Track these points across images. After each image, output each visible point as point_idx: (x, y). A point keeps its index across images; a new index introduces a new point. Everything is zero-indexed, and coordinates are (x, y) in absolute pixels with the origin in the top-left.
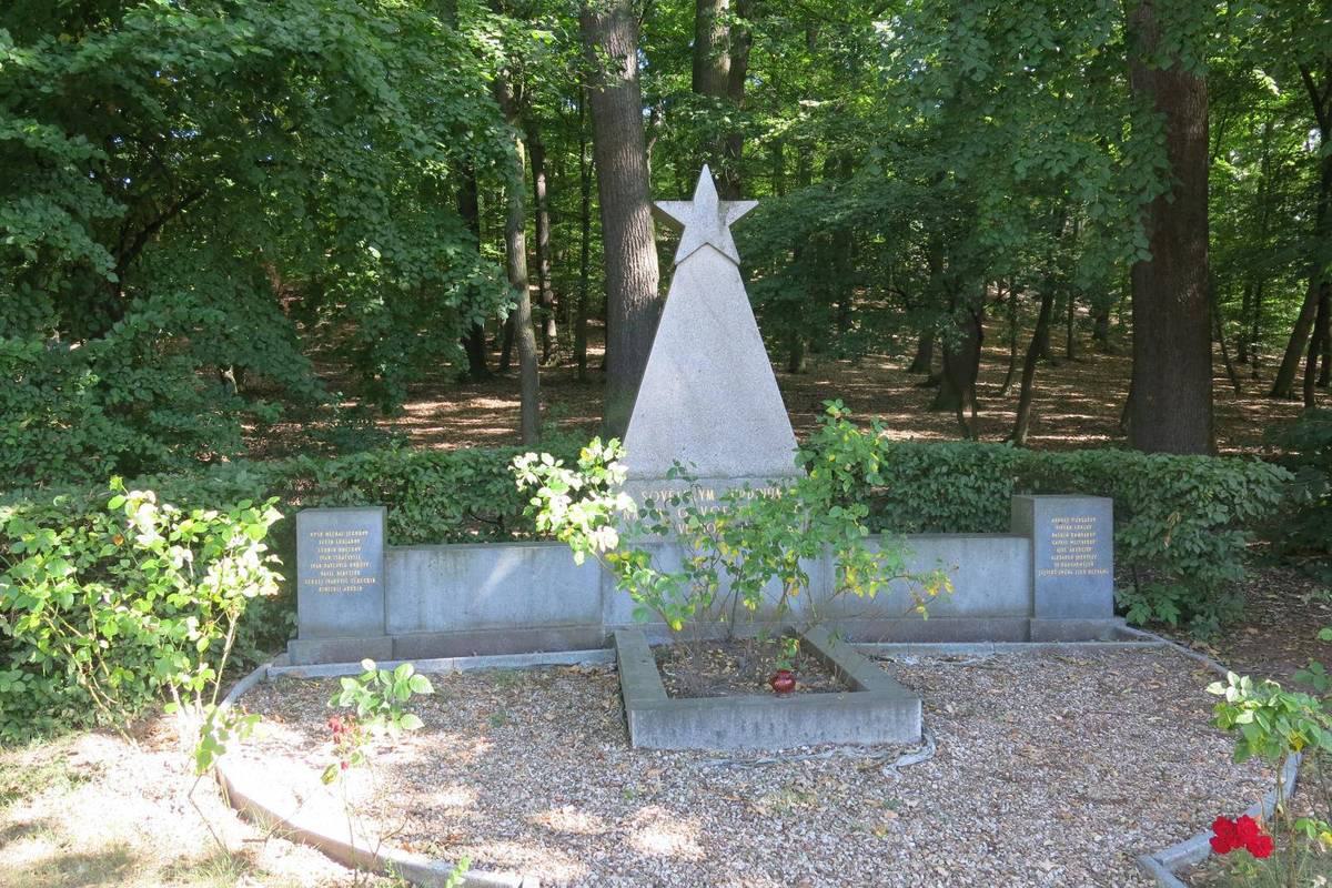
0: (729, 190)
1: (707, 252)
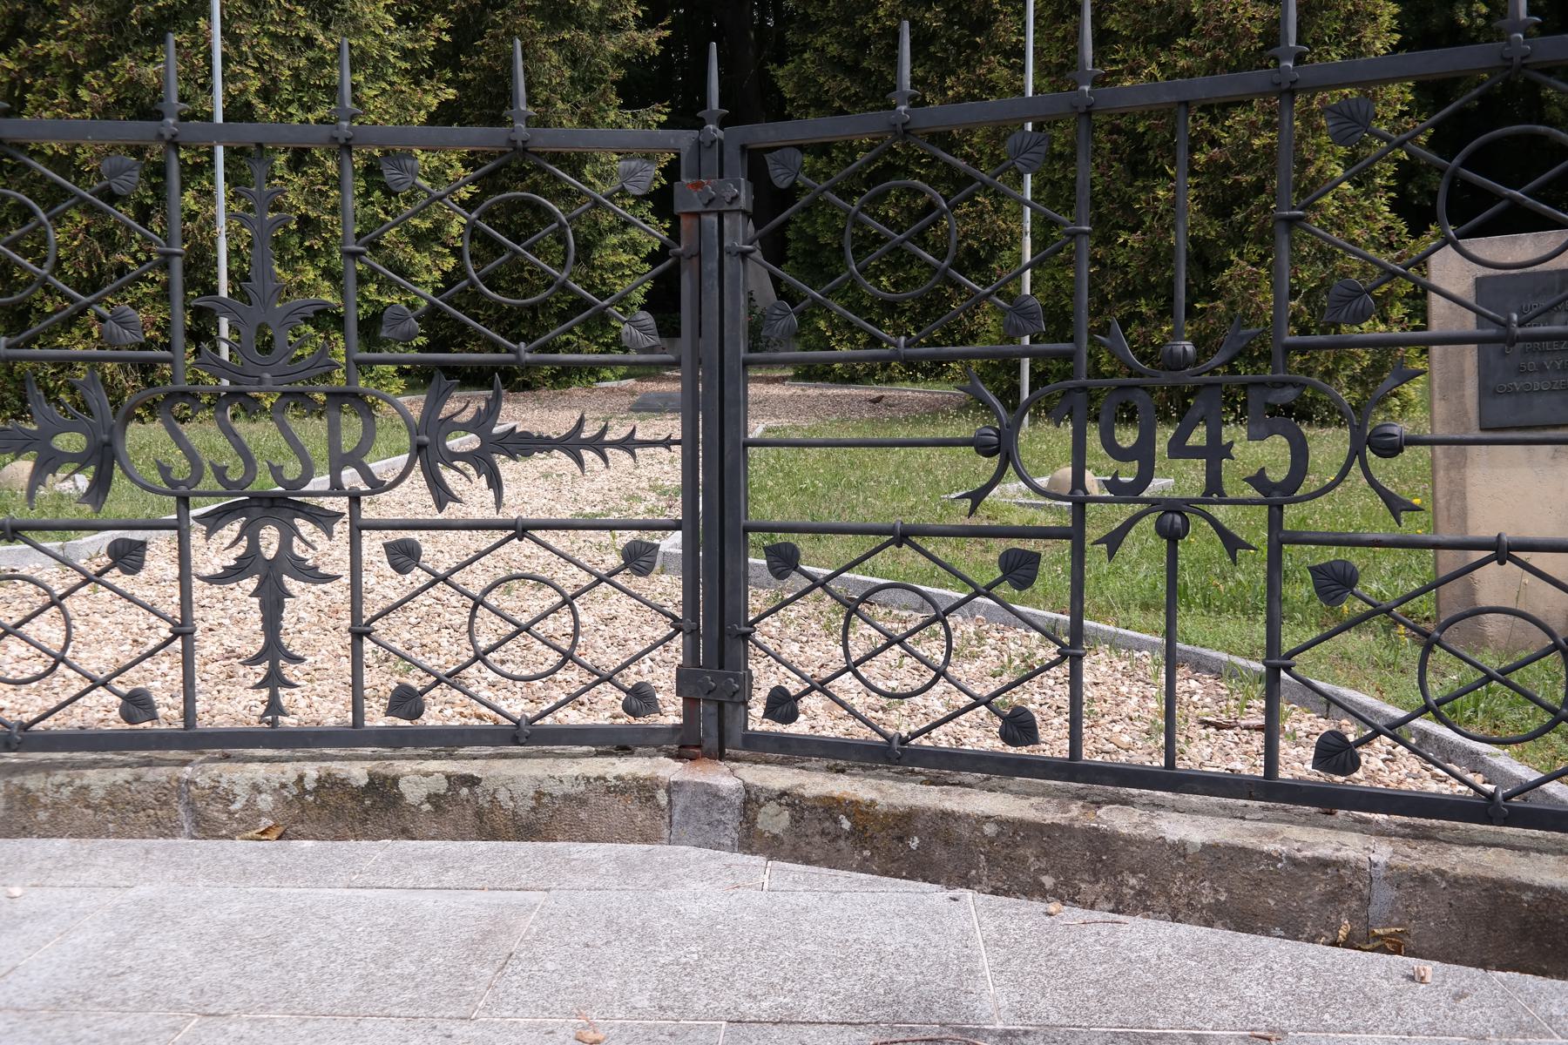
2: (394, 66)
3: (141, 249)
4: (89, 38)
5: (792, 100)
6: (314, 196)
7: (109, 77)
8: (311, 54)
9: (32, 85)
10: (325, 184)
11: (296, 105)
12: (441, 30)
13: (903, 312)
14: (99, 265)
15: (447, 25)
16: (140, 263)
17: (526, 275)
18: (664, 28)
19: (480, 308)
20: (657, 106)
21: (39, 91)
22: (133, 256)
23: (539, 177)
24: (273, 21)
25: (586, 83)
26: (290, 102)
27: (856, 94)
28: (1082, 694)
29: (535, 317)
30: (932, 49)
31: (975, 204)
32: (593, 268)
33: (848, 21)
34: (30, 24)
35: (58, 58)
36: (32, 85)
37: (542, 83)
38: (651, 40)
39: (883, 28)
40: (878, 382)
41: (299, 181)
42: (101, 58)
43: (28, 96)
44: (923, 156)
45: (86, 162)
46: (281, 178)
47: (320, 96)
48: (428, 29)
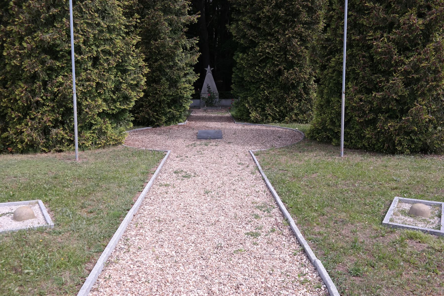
0: (211, 67)
2: (123, 31)
3: (44, 95)
4: (26, 25)
5: (236, 36)
6: (101, 76)
7: (33, 38)
8: (98, 28)
9: (6, 41)
10: (104, 72)
11: (94, 45)
12: (137, 19)
13: (271, 102)
14: (30, 101)
15: (139, 17)
16: (44, 100)
17: (158, 92)
18: (198, 14)
19: (144, 102)
20: (195, 38)
21: (9, 43)
22: (42, 97)
23: (162, 62)
24: (87, 18)
25: (174, 31)
26: (92, 45)
29: (160, 104)
30: (280, 22)
31: (294, 69)
32: (178, 89)
33: (253, 12)
34: (5, 19)
35: (15, 32)
36: (6, 41)
37: (163, 32)
38: (195, 18)
39: (265, 15)
40: (265, 123)
41: (96, 71)
42: (30, 32)
43: (5, 45)
44: (278, 55)
45: (25, 68)
46: (90, 70)
47: (102, 42)
48: (133, 18)
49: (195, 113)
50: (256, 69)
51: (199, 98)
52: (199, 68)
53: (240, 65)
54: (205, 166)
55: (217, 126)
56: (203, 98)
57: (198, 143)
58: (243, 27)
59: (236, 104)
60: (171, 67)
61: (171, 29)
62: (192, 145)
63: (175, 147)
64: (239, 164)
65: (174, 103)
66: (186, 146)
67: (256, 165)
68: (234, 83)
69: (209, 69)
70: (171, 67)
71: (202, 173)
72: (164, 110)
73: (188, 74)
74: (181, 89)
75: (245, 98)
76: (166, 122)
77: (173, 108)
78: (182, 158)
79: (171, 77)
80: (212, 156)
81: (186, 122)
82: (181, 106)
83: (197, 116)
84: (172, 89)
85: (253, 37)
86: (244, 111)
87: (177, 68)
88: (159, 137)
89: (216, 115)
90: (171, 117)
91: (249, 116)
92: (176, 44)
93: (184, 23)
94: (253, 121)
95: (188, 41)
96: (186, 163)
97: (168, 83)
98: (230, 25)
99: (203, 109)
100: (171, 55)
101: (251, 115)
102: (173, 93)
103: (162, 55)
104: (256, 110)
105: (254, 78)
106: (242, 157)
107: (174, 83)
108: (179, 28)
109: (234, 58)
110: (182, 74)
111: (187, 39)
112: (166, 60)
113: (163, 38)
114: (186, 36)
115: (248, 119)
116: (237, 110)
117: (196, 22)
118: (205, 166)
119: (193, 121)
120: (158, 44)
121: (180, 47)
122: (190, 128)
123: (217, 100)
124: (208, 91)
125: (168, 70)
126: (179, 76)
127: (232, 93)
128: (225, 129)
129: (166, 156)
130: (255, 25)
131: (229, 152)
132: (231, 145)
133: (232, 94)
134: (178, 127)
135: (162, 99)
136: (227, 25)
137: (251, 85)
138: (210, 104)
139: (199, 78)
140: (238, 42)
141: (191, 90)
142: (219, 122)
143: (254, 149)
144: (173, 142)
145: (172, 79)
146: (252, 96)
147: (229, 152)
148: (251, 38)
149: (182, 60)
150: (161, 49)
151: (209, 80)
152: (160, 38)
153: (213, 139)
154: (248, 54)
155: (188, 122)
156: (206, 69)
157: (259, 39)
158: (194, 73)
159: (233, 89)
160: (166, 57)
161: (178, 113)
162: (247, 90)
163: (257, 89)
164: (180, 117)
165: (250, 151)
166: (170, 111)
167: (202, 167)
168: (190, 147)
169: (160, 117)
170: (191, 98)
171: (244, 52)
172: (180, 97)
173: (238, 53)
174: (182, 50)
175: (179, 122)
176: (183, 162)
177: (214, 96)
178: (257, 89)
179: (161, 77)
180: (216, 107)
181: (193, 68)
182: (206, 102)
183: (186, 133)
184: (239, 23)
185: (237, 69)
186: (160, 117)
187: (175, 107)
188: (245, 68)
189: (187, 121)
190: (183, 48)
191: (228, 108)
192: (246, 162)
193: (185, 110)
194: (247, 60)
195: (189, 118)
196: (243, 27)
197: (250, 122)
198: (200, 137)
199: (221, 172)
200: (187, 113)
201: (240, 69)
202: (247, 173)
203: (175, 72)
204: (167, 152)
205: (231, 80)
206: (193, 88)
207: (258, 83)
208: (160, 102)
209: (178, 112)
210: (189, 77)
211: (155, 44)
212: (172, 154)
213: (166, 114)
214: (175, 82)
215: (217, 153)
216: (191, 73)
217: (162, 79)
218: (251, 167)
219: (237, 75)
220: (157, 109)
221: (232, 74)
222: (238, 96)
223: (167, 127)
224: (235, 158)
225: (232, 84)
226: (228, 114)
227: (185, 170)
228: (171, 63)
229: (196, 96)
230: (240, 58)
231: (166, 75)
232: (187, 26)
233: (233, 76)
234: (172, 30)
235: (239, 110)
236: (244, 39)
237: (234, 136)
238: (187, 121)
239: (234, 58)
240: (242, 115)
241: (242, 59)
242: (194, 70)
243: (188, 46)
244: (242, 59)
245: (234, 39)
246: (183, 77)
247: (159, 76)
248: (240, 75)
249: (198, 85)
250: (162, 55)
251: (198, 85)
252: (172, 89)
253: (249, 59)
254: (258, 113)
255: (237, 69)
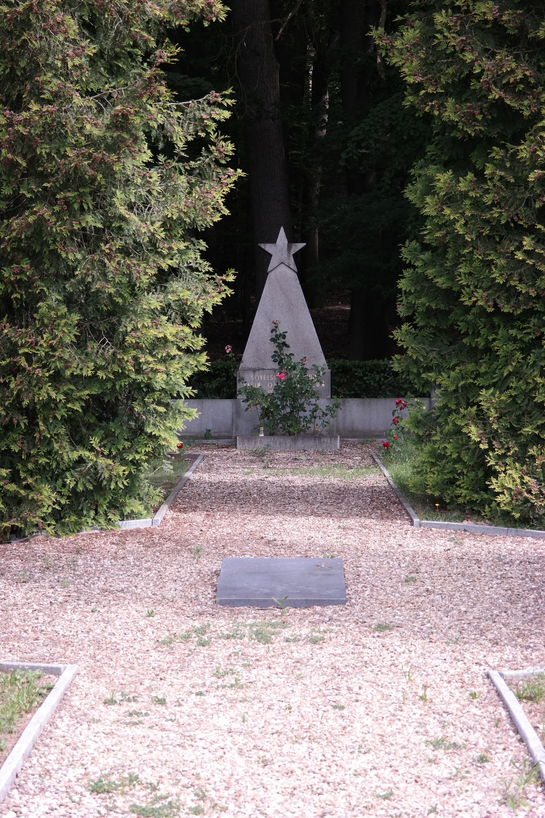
0: (291, 240)
1: (283, 268)
5: (419, 86)
17: (23, 362)
20: (213, 96)
23: (45, 211)
25: (110, 63)
27: (525, 80)
28: (243, 606)
29: (33, 424)
32: (123, 347)
37: (52, 67)
49: (209, 469)
50: (520, 247)
51: (232, 395)
52: (232, 247)
53: (440, 227)
54: (255, 755)
55: (319, 538)
56: (252, 394)
57: (222, 624)
58: (455, 41)
59: (418, 423)
60: (89, 240)
61: (92, 50)
62: (186, 638)
63: (98, 644)
64: (437, 744)
65: (100, 419)
66: (160, 644)
67: (529, 752)
68: (410, 319)
69: (281, 252)
70: (89, 240)
71: (237, 795)
72: (49, 453)
73: (174, 271)
74: (137, 346)
75: (466, 395)
76: (58, 516)
77: (95, 441)
78: (134, 707)
79: (88, 287)
80: (295, 700)
81: (159, 517)
82: (138, 432)
83: (217, 486)
84: (92, 346)
85: (507, 87)
86: (459, 460)
87: (119, 244)
88: (18, 594)
89: (317, 479)
90: (86, 492)
91: (486, 489)
92: (121, 123)
93: (161, 22)
94: (506, 514)
95: (179, 109)
96: (156, 734)
97: (76, 317)
98: (392, 28)
99: (251, 446)
100: (93, 179)
101: (495, 484)
102: (97, 368)
103: (44, 177)
104: (522, 458)
105: (511, 293)
106: (453, 708)
107: (102, 320)
108: (135, 45)
109: (411, 194)
110: (145, 273)
111: (177, 99)
112: (67, 203)
113: (56, 95)
114: (171, 86)
115: (483, 503)
116: (423, 457)
117: (223, 17)
118: (255, 755)
119: (195, 509)
120: (26, 123)
121: (136, 139)
122: (182, 545)
123: (323, 403)
124: (278, 358)
125: (73, 255)
126: (132, 286)
127: (396, 367)
128: (361, 552)
129: (53, 699)
130: (522, 28)
131: (383, 679)
132: (393, 640)
133: (396, 374)
134: (122, 543)
135: (43, 396)
136: (377, 33)
137: (493, 328)
138: (284, 418)
139: (230, 292)
140: (428, 118)
141: (188, 351)
142: (329, 514)
143: (514, 665)
144: (91, 618)
145: (93, 297)
146: (501, 385)
147: (383, 679)
148: (496, 94)
149: (146, 203)
150: (43, 150)
151: (284, 304)
152: (37, 93)
153: (296, 605)
154: (480, 175)
155: (171, 514)
156: (268, 248)
157: (537, 97)
158: (206, 266)
159: (402, 351)
160: (64, 187)
161: (121, 469)
162: (473, 353)
163: (526, 350)
164: (130, 491)
165: (495, 675)
166: (81, 461)
167: (241, 761)
168: (180, 649)
169: (28, 487)
170: (189, 391)
171: (458, 163)
172: (135, 386)
173: (431, 170)
174: (147, 156)
175: (123, 517)
176: (138, 731)
177: (303, 381)
178: (526, 350)
179: (40, 286)
180: (316, 436)
181: (203, 245)
182: (266, 413)
183: (160, 576)
184: (440, 18)
185: (425, 247)
186: (28, 487)
187: (109, 437)
188: (465, 244)
189: (164, 511)
190: (153, 148)
191: (379, 442)
192: (474, 737)
193: (154, 455)
194: (477, 204)
195: (175, 493)
196: (455, 41)
197: (492, 520)
198: (230, 596)
199: (338, 786)
200: (168, 467)
201: (438, 251)
202: (479, 796)
203: (111, 266)
204: (57, 672)
205: (392, 302)
206: (200, 342)
207: (534, 321)
208: (31, 413)
209: (123, 462)
210: (180, 290)
211: (10, 124)
212: (84, 683)
213: (61, 475)
214: (111, 313)
215: (318, 679)
216: (193, 269)
217: (42, 296)
218: (502, 762)
219: (424, 283)
220: (15, 448)
221: (397, 275)
222: (427, 383)
223: (63, 540)
224: (414, 711)
225: (399, 322)
226: (379, 477)
227: (148, 776)
228: (92, 221)
229: (217, 382)
230: (437, 193)
231: (66, 278)
232: (174, 35)
233: (403, 284)
234: (100, 54)
235: (433, 453)
236: (460, 101)
237: (408, 589)
238: (164, 511)
239: (411, 194)
240: (452, 482)
241: (451, 199)
242: (204, 255)
243: (180, 137)
244: (451, 199)
245: (409, 100)
246: (152, 287)
247: (28, 285)
248: (440, 282)
249: (227, 328)
250: (44, 177)
251: (227, 328)
252: (92, 346)
253: (488, 199)
254: (531, 474)
255: (425, 247)
